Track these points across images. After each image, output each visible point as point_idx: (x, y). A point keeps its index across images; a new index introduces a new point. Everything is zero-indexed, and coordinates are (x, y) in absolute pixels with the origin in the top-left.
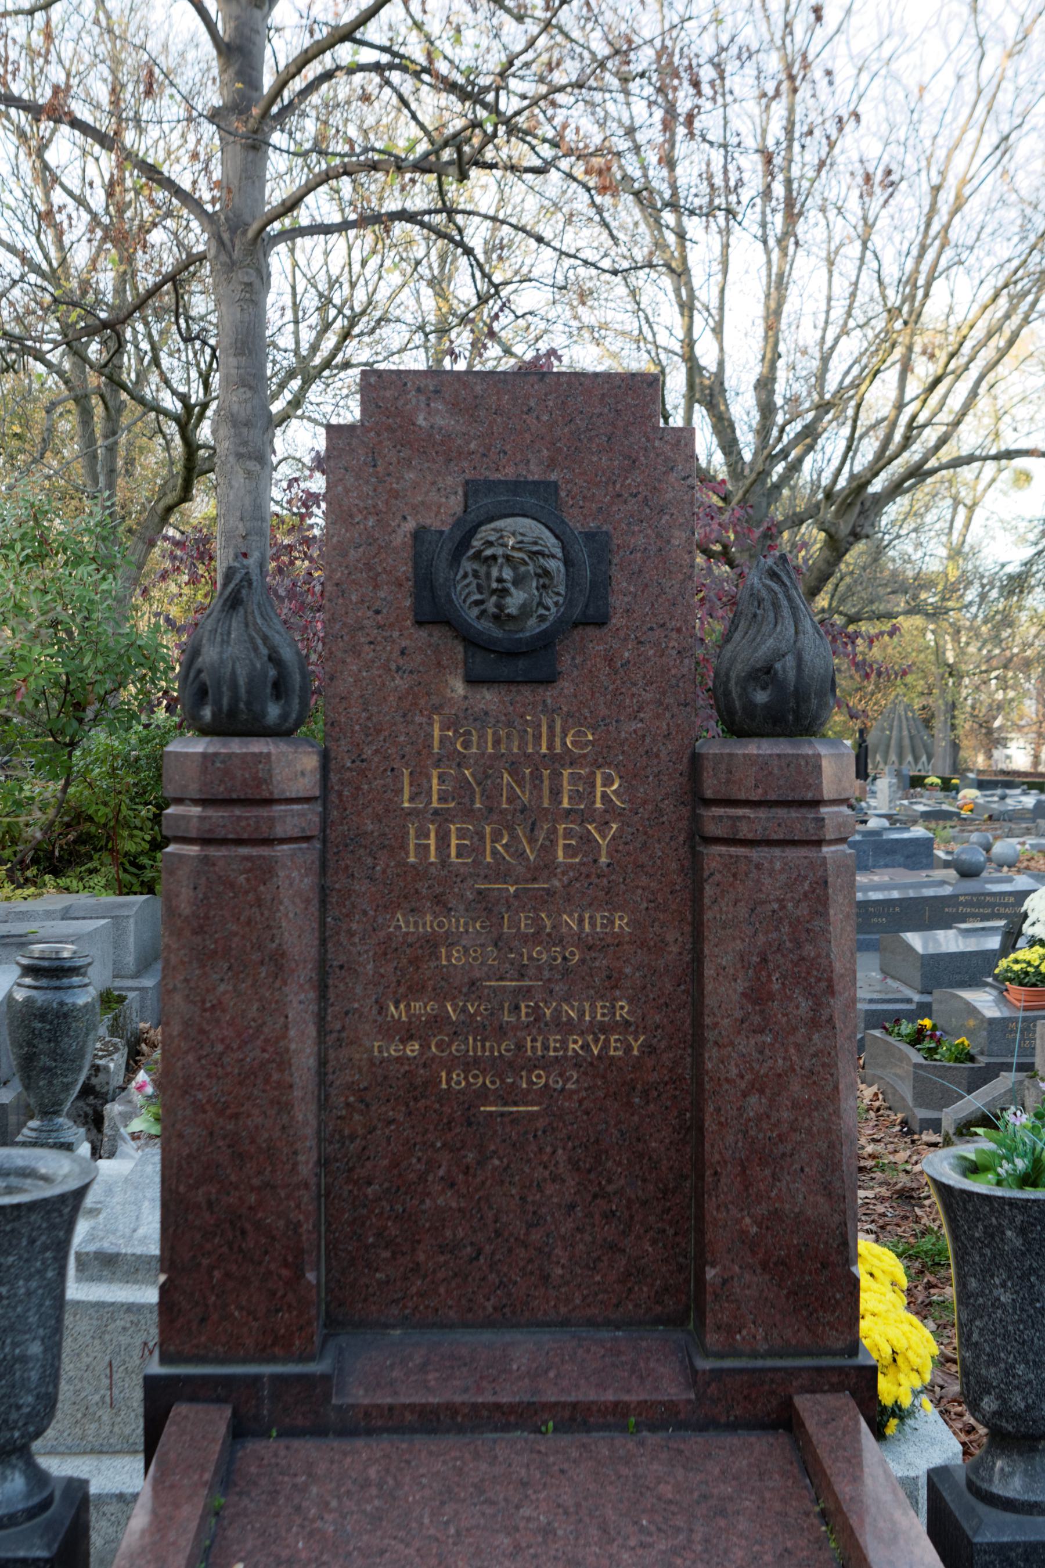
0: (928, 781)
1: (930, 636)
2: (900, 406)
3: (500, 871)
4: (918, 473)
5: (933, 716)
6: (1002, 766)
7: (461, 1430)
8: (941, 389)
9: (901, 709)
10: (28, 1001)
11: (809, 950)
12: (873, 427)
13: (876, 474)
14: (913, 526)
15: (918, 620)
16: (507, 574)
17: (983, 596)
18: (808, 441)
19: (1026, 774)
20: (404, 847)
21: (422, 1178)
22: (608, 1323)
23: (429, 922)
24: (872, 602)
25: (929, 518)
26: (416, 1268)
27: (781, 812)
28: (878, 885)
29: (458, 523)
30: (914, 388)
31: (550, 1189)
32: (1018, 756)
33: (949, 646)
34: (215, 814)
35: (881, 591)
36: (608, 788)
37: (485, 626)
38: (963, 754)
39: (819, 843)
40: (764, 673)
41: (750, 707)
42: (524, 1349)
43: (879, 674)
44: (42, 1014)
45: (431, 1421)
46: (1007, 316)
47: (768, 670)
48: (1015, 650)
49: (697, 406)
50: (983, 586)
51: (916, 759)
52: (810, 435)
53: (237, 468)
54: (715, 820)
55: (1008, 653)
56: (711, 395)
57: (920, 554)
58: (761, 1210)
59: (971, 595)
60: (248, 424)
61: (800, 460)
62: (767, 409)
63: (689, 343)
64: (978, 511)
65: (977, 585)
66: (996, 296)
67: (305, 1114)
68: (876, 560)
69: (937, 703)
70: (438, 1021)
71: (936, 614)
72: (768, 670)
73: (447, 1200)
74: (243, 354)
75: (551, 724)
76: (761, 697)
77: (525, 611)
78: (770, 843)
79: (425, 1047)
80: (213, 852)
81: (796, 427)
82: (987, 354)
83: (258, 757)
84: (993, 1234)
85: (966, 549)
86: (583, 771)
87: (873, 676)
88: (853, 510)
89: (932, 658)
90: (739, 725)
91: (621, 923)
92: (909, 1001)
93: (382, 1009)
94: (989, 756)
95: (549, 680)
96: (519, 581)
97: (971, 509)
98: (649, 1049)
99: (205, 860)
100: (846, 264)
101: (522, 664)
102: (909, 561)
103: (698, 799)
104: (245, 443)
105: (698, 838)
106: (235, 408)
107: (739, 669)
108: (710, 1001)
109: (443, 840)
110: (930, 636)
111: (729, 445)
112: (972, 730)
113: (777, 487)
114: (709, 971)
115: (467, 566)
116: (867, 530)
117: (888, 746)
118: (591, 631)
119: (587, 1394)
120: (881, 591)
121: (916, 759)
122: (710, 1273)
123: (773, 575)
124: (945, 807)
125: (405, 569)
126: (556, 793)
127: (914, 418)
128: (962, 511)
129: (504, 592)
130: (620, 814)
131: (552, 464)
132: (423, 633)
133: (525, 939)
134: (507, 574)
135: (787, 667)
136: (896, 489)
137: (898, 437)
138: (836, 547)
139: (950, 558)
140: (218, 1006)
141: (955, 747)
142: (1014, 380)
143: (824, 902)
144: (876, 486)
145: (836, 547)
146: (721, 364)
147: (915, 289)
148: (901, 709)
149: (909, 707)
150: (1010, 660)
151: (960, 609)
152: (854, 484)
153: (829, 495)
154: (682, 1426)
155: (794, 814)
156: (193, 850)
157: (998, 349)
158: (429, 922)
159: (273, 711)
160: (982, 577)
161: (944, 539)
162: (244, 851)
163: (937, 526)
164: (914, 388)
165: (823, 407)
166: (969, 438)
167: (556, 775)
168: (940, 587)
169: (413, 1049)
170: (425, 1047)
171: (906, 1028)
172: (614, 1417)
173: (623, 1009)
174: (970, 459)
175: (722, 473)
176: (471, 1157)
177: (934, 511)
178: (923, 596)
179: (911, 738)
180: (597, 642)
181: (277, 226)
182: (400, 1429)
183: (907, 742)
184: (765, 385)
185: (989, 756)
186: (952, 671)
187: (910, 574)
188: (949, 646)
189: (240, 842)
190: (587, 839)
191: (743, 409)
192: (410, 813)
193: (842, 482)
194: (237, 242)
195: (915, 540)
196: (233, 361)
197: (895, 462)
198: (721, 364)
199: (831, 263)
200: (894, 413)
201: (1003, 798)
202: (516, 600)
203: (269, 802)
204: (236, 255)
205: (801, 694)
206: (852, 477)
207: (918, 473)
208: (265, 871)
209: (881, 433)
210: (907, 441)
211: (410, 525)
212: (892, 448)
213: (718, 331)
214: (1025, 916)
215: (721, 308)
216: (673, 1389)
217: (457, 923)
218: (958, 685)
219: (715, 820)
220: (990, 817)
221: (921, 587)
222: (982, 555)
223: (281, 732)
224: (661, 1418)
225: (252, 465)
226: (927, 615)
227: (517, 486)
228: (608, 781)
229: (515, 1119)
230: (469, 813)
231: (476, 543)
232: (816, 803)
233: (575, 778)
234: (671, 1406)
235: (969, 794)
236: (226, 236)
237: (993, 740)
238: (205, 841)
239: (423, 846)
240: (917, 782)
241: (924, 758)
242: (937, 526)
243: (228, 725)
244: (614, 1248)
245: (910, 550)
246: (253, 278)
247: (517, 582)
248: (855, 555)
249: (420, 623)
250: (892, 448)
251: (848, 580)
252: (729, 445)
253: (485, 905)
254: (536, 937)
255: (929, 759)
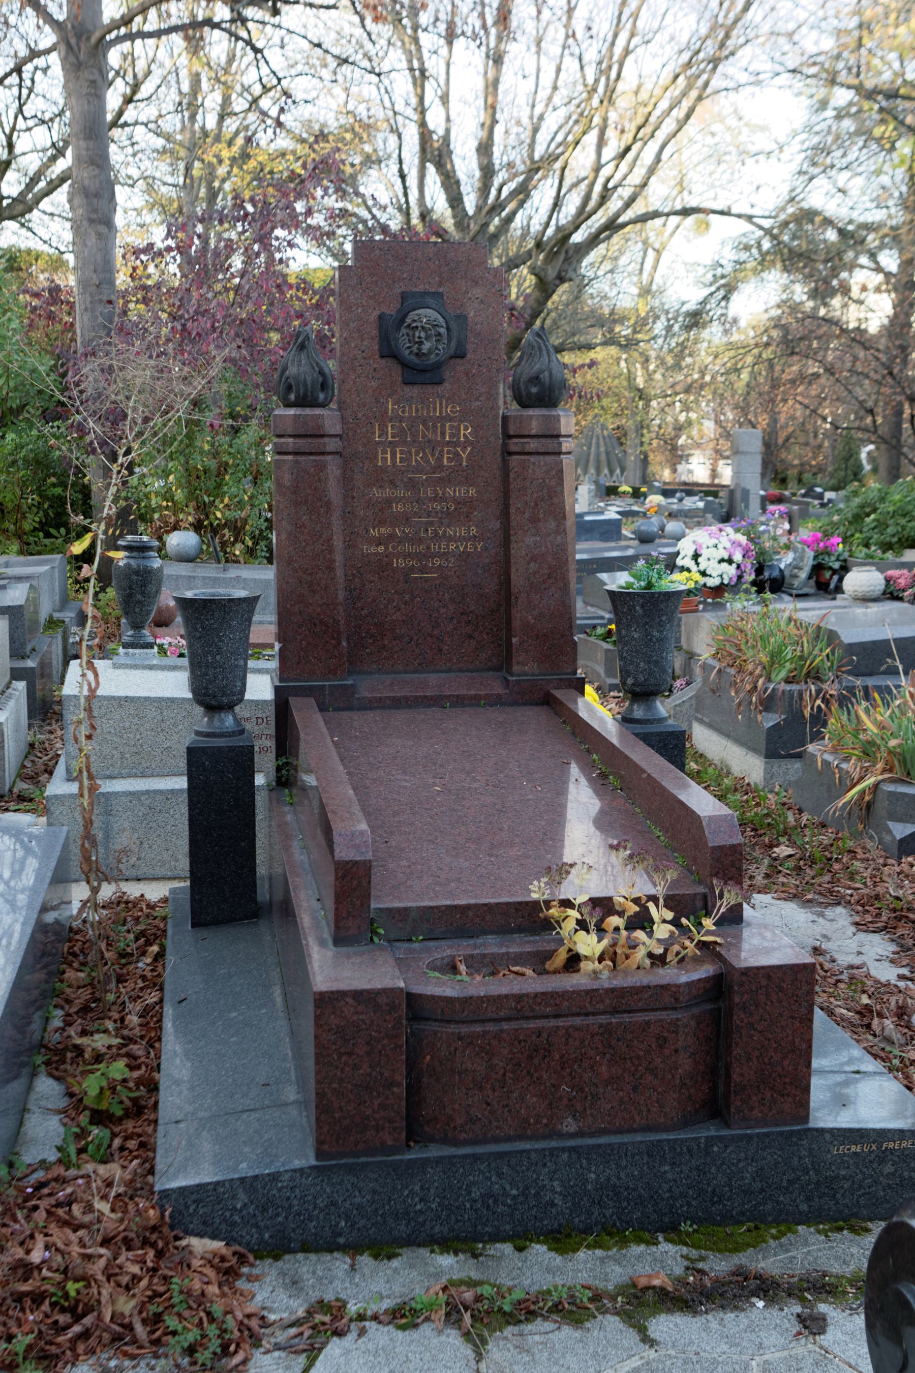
0: (621, 489)
1: (623, 364)
2: (597, 169)
3: (419, 470)
4: (612, 227)
5: (625, 435)
6: (684, 478)
7: (410, 707)
8: (630, 156)
9: (598, 430)
10: (128, 565)
11: (556, 500)
12: (575, 185)
13: (577, 228)
14: (609, 267)
15: (613, 350)
16: (423, 335)
17: (669, 328)
18: (521, 196)
19: (703, 485)
20: (376, 458)
21: (386, 607)
22: (468, 671)
23: (387, 492)
24: (574, 334)
25: (623, 261)
26: (384, 647)
27: (543, 440)
28: (583, 551)
29: (399, 311)
30: (609, 153)
31: (442, 611)
32: (698, 469)
33: (639, 373)
34: (301, 441)
35: (582, 326)
36: (466, 431)
37: (413, 357)
38: (651, 468)
39: (560, 453)
40: (535, 379)
41: (529, 394)
42: (433, 679)
43: (580, 397)
44: (137, 573)
45: (397, 703)
46: (684, 94)
47: (537, 378)
48: (696, 376)
49: (428, 164)
50: (668, 320)
51: (612, 472)
52: (523, 192)
53: (90, 230)
54: (515, 445)
55: (689, 380)
56: (440, 156)
57: (614, 292)
58: (535, 613)
59: (659, 327)
60: (97, 195)
61: (514, 213)
62: (488, 172)
63: (422, 110)
64: (664, 255)
65: (663, 318)
66: (676, 77)
67: (340, 573)
68: (577, 298)
69: (629, 424)
70: (392, 537)
71: (629, 345)
72: (537, 378)
73: (397, 616)
74: (90, 138)
75: (440, 404)
76: (534, 390)
77: (430, 351)
78: (538, 453)
79: (387, 548)
80: (299, 458)
81: (512, 185)
82: (669, 126)
83: (319, 416)
84: (632, 609)
85: (654, 288)
86: (455, 422)
87: (575, 398)
88: (560, 256)
89: (625, 383)
90: (524, 401)
91: (472, 492)
92: (602, 618)
93: (367, 531)
94: (674, 471)
95: (440, 383)
96: (428, 338)
97: (658, 252)
98: (485, 549)
99: (297, 462)
100: (552, 48)
101: (428, 375)
102: (605, 297)
103: (507, 436)
104: (95, 211)
105: (507, 453)
106: (86, 182)
107: (524, 378)
108: (513, 524)
109: (394, 455)
110: (623, 364)
111: (455, 200)
112: (659, 446)
113: (495, 237)
114: (512, 510)
115: (404, 331)
116: (571, 274)
117: (588, 461)
118: (458, 361)
119: (463, 692)
120: (582, 326)
121: (612, 472)
122: (514, 640)
123: (538, 335)
124: (635, 508)
125: (375, 332)
126: (443, 434)
127: (608, 180)
128: (651, 254)
129: (421, 343)
130: (471, 443)
131: (440, 284)
132: (383, 361)
133: (430, 500)
134: (423, 335)
135: (545, 376)
136: (594, 241)
137: (595, 196)
138: (545, 288)
139: (640, 295)
140: (303, 526)
141: (645, 462)
142: (693, 144)
143: (561, 479)
144: (577, 237)
145: (545, 288)
146: (448, 131)
147: (610, 69)
148: (598, 430)
149: (604, 427)
150: (690, 386)
151: (648, 341)
152: (560, 235)
153: (539, 245)
154: (503, 704)
155: (549, 441)
156: (290, 457)
157: (678, 121)
158: (387, 492)
159: (322, 396)
160: (667, 312)
161: (635, 279)
162: (312, 458)
163: (630, 268)
164: (609, 153)
165: (534, 169)
166: (658, 194)
167: (443, 426)
168: (632, 322)
169: (381, 549)
170: (387, 548)
171: (600, 631)
172: (473, 701)
173: (474, 530)
174: (656, 215)
175: (449, 223)
176: (407, 597)
177: (628, 254)
178: (617, 329)
179: (607, 453)
180: (460, 366)
181: (113, 35)
182: (383, 708)
183: (603, 457)
184: (485, 149)
185: (674, 471)
186: (641, 394)
187: (606, 311)
188: (639, 373)
189: (311, 454)
190: (457, 454)
191: (466, 166)
192: (378, 443)
193: (550, 231)
194: (83, 46)
195: (612, 280)
196: (83, 144)
197: (594, 217)
198: (448, 131)
199: (538, 43)
200: (592, 175)
201: (681, 500)
202: (426, 346)
203: (323, 436)
204: (82, 57)
205: (551, 388)
206: (558, 229)
207: (612, 227)
208: (322, 467)
209: (583, 186)
210: (604, 199)
211: (376, 313)
212: (592, 204)
213: (445, 99)
214: (678, 553)
215: (448, 80)
216: (498, 689)
217: (400, 493)
218: (647, 405)
219: (515, 445)
220: (670, 515)
221: (615, 321)
222: (668, 293)
223: (322, 406)
224: (495, 701)
225: (102, 229)
226: (621, 346)
227: (425, 294)
228: (466, 428)
229: (426, 580)
230: (405, 443)
231: (408, 321)
232: (558, 436)
233: (451, 427)
234: (499, 696)
235: (655, 499)
236: (73, 41)
237: (676, 456)
238: (295, 453)
239: (385, 458)
240: (612, 491)
241: (618, 471)
242: (630, 268)
243: (301, 402)
244: (471, 637)
245: (607, 289)
246: (97, 76)
247: (427, 338)
248: (561, 295)
249: (382, 357)
250: (592, 204)
251: (553, 314)
252: (455, 200)
253: (412, 485)
254: (435, 499)
255: (622, 472)
